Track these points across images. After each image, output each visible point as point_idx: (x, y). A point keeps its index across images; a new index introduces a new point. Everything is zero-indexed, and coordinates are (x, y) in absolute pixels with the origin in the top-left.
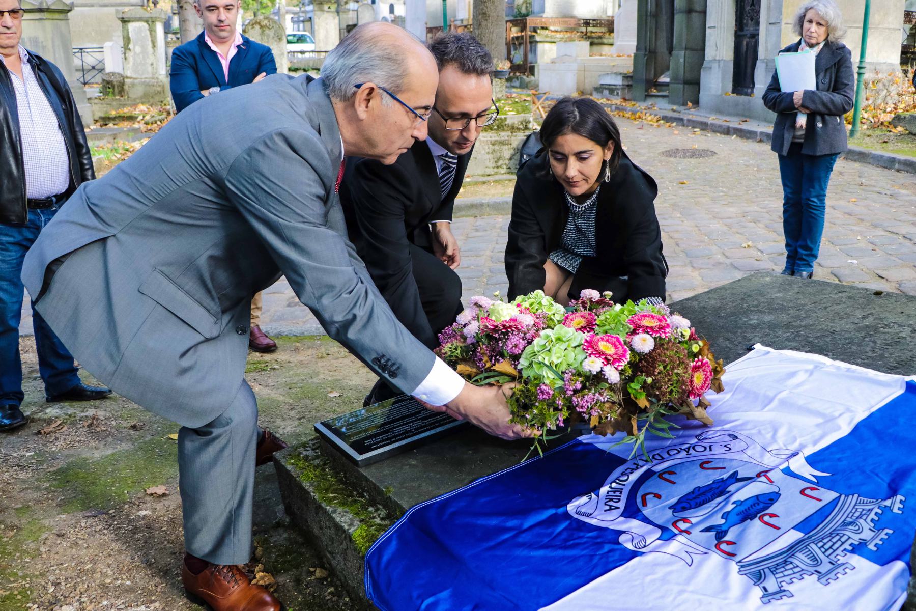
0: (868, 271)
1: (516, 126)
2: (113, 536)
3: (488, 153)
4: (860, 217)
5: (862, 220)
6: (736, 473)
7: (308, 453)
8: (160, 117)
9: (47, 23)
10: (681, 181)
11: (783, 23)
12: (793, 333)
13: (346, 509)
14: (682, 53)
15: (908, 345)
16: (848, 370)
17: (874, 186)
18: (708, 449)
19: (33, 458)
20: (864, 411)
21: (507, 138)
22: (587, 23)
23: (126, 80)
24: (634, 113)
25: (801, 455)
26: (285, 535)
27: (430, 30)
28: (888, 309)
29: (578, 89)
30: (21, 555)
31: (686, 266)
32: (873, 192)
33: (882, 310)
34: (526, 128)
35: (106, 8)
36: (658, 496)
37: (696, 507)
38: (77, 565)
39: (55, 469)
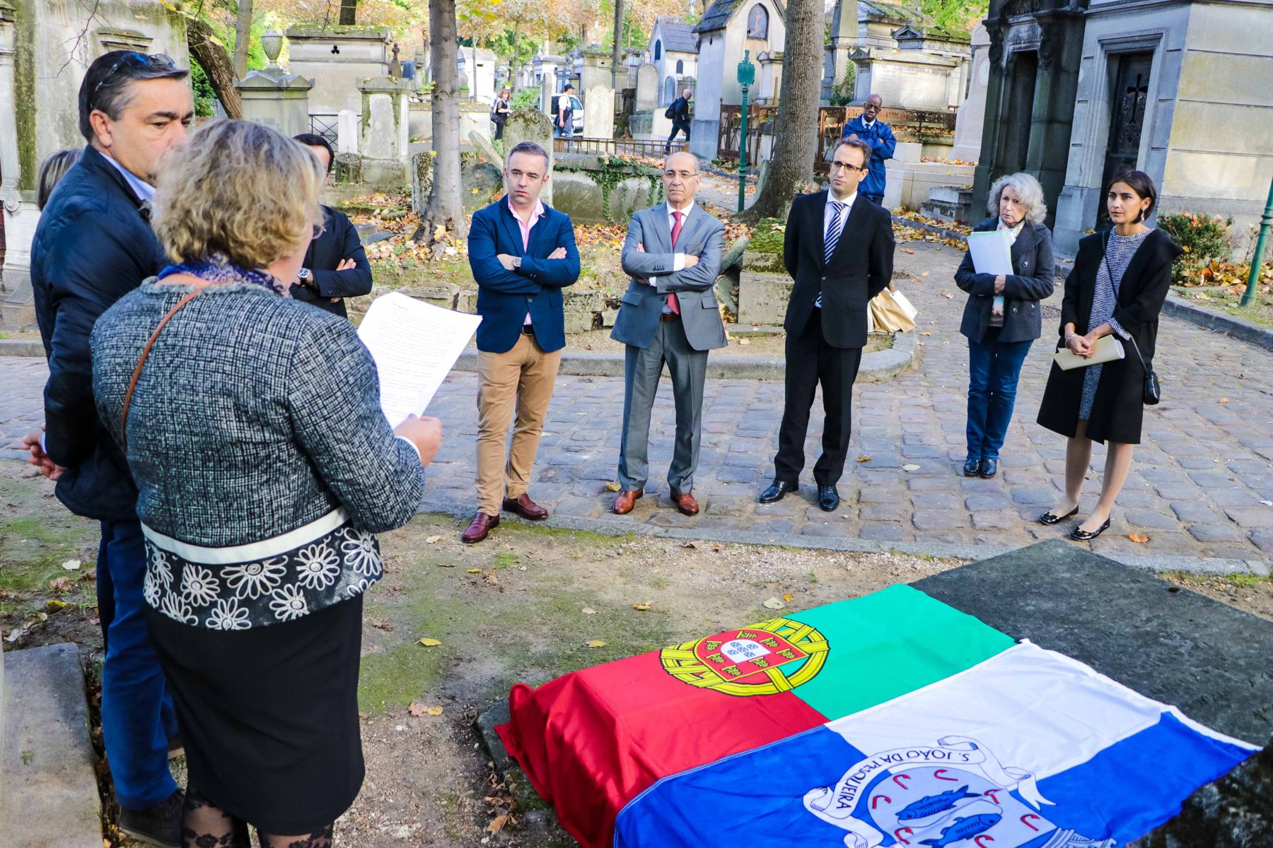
0: (1216, 509)
3: (782, 299)
4: (1226, 428)
5: (1228, 433)
6: (966, 787)
8: (400, 213)
9: (285, 103)
11: (1169, 149)
12: (1066, 629)
15: (1183, 664)
16: (1109, 686)
17: (1259, 381)
22: (921, 116)
23: (363, 161)
27: (725, 108)
29: (902, 204)
32: (1254, 389)
35: (342, 65)
36: (888, 800)
37: (921, 817)
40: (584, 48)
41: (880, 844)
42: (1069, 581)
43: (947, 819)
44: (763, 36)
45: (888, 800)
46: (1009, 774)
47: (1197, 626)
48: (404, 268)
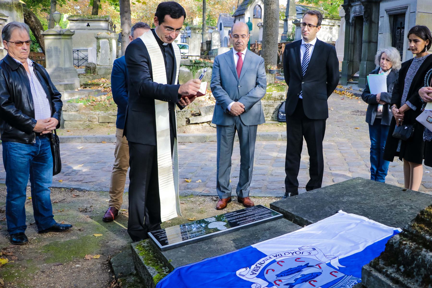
1: (277, 97)
2: (64, 274)
7: (145, 245)
9: (62, 40)
10: (356, 127)
12: (359, 206)
13: (154, 268)
14: (366, 62)
15: (405, 214)
16: (374, 224)
18: (301, 253)
19: (36, 240)
20: (371, 242)
21: (272, 103)
24: (341, 91)
25: (337, 258)
26: (133, 278)
28: (405, 198)
30: (27, 278)
31: (346, 170)
33: (402, 198)
34: (282, 99)
35: (91, 31)
36: (273, 270)
38: (48, 284)
39: (44, 245)
40: (191, 26)
41: (266, 287)
42: (363, 191)
43: (298, 275)
44: (260, 17)
45: (273, 270)
46: (327, 258)
47: (413, 201)
48: (110, 104)
